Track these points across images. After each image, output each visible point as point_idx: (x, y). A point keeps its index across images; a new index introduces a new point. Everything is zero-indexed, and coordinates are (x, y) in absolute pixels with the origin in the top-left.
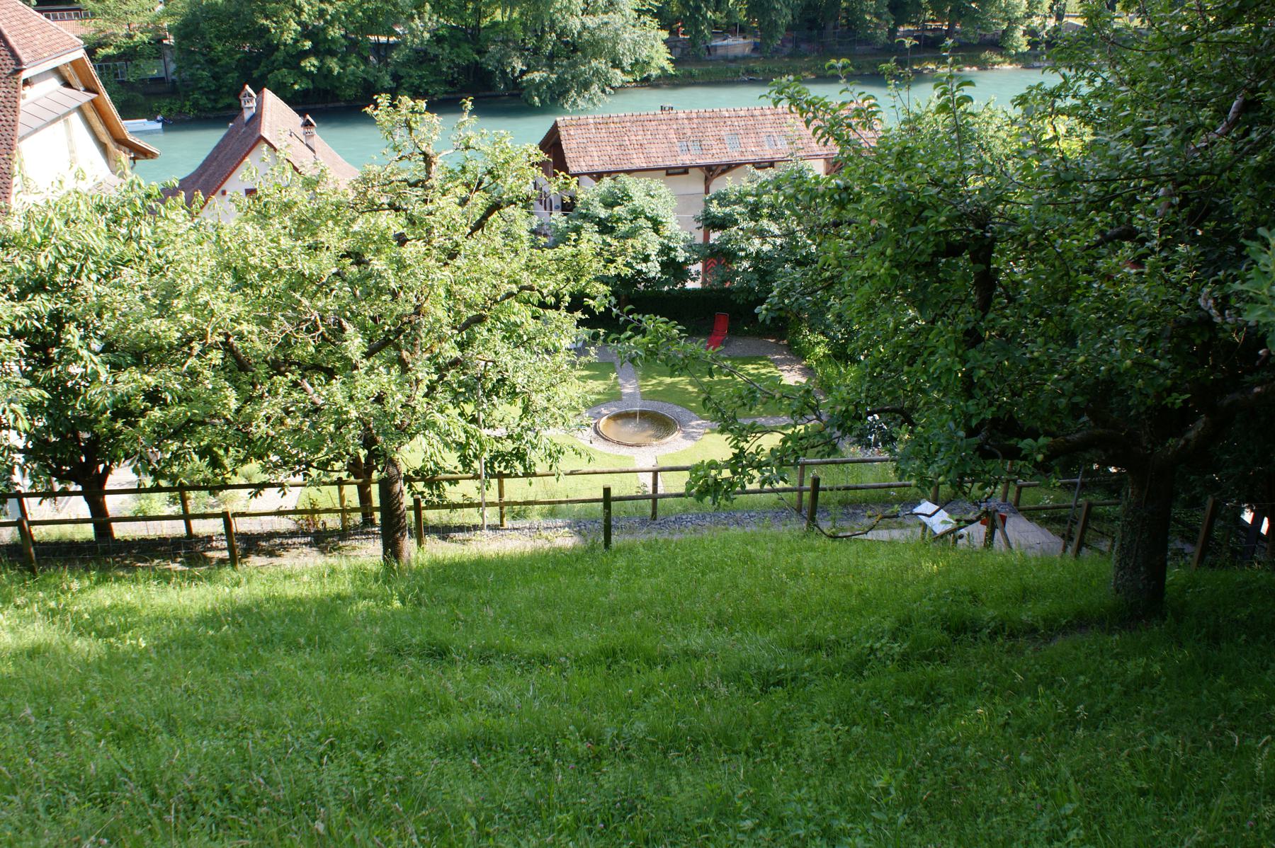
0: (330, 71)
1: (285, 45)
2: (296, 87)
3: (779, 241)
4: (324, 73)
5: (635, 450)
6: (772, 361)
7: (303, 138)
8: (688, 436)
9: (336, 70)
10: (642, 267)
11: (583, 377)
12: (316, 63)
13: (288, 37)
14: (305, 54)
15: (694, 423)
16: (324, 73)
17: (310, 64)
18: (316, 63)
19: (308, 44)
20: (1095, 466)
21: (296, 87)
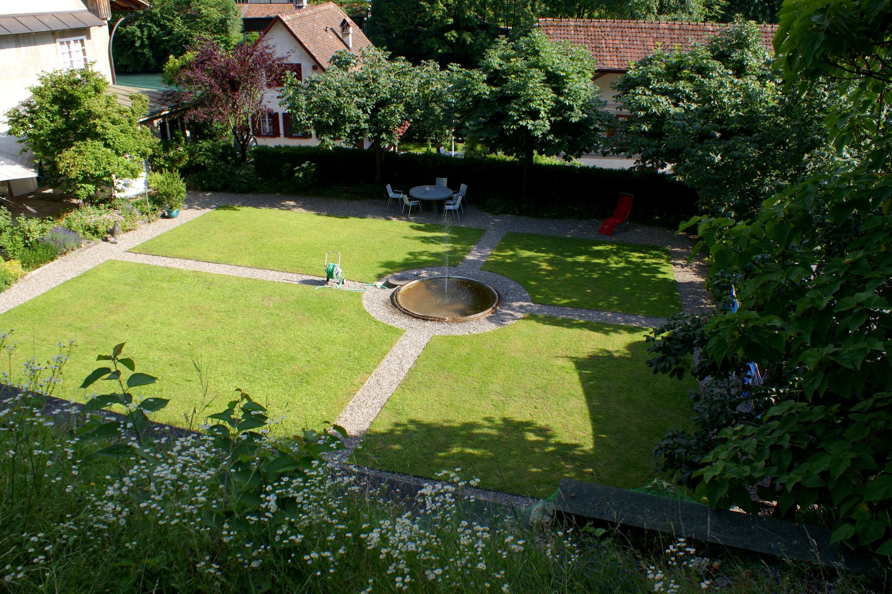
0: (465, 41)
1: (436, 21)
2: (440, 51)
3: (694, 106)
4: (460, 41)
5: (416, 323)
6: (667, 252)
7: (340, 35)
8: (496, 318)
9: (469, 40)
10: (529, 124)
11: (425, 238)
12: (455, 35)
13: (437, 15)
14: (449, 28)
15: (516, 304)
16: (460, 41)
17: (451, 36)
18: (455, 35)
19: (451, 21)
20: (319, 573)
21: (440, 51)
